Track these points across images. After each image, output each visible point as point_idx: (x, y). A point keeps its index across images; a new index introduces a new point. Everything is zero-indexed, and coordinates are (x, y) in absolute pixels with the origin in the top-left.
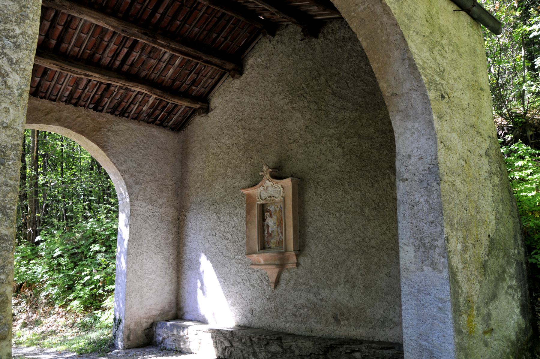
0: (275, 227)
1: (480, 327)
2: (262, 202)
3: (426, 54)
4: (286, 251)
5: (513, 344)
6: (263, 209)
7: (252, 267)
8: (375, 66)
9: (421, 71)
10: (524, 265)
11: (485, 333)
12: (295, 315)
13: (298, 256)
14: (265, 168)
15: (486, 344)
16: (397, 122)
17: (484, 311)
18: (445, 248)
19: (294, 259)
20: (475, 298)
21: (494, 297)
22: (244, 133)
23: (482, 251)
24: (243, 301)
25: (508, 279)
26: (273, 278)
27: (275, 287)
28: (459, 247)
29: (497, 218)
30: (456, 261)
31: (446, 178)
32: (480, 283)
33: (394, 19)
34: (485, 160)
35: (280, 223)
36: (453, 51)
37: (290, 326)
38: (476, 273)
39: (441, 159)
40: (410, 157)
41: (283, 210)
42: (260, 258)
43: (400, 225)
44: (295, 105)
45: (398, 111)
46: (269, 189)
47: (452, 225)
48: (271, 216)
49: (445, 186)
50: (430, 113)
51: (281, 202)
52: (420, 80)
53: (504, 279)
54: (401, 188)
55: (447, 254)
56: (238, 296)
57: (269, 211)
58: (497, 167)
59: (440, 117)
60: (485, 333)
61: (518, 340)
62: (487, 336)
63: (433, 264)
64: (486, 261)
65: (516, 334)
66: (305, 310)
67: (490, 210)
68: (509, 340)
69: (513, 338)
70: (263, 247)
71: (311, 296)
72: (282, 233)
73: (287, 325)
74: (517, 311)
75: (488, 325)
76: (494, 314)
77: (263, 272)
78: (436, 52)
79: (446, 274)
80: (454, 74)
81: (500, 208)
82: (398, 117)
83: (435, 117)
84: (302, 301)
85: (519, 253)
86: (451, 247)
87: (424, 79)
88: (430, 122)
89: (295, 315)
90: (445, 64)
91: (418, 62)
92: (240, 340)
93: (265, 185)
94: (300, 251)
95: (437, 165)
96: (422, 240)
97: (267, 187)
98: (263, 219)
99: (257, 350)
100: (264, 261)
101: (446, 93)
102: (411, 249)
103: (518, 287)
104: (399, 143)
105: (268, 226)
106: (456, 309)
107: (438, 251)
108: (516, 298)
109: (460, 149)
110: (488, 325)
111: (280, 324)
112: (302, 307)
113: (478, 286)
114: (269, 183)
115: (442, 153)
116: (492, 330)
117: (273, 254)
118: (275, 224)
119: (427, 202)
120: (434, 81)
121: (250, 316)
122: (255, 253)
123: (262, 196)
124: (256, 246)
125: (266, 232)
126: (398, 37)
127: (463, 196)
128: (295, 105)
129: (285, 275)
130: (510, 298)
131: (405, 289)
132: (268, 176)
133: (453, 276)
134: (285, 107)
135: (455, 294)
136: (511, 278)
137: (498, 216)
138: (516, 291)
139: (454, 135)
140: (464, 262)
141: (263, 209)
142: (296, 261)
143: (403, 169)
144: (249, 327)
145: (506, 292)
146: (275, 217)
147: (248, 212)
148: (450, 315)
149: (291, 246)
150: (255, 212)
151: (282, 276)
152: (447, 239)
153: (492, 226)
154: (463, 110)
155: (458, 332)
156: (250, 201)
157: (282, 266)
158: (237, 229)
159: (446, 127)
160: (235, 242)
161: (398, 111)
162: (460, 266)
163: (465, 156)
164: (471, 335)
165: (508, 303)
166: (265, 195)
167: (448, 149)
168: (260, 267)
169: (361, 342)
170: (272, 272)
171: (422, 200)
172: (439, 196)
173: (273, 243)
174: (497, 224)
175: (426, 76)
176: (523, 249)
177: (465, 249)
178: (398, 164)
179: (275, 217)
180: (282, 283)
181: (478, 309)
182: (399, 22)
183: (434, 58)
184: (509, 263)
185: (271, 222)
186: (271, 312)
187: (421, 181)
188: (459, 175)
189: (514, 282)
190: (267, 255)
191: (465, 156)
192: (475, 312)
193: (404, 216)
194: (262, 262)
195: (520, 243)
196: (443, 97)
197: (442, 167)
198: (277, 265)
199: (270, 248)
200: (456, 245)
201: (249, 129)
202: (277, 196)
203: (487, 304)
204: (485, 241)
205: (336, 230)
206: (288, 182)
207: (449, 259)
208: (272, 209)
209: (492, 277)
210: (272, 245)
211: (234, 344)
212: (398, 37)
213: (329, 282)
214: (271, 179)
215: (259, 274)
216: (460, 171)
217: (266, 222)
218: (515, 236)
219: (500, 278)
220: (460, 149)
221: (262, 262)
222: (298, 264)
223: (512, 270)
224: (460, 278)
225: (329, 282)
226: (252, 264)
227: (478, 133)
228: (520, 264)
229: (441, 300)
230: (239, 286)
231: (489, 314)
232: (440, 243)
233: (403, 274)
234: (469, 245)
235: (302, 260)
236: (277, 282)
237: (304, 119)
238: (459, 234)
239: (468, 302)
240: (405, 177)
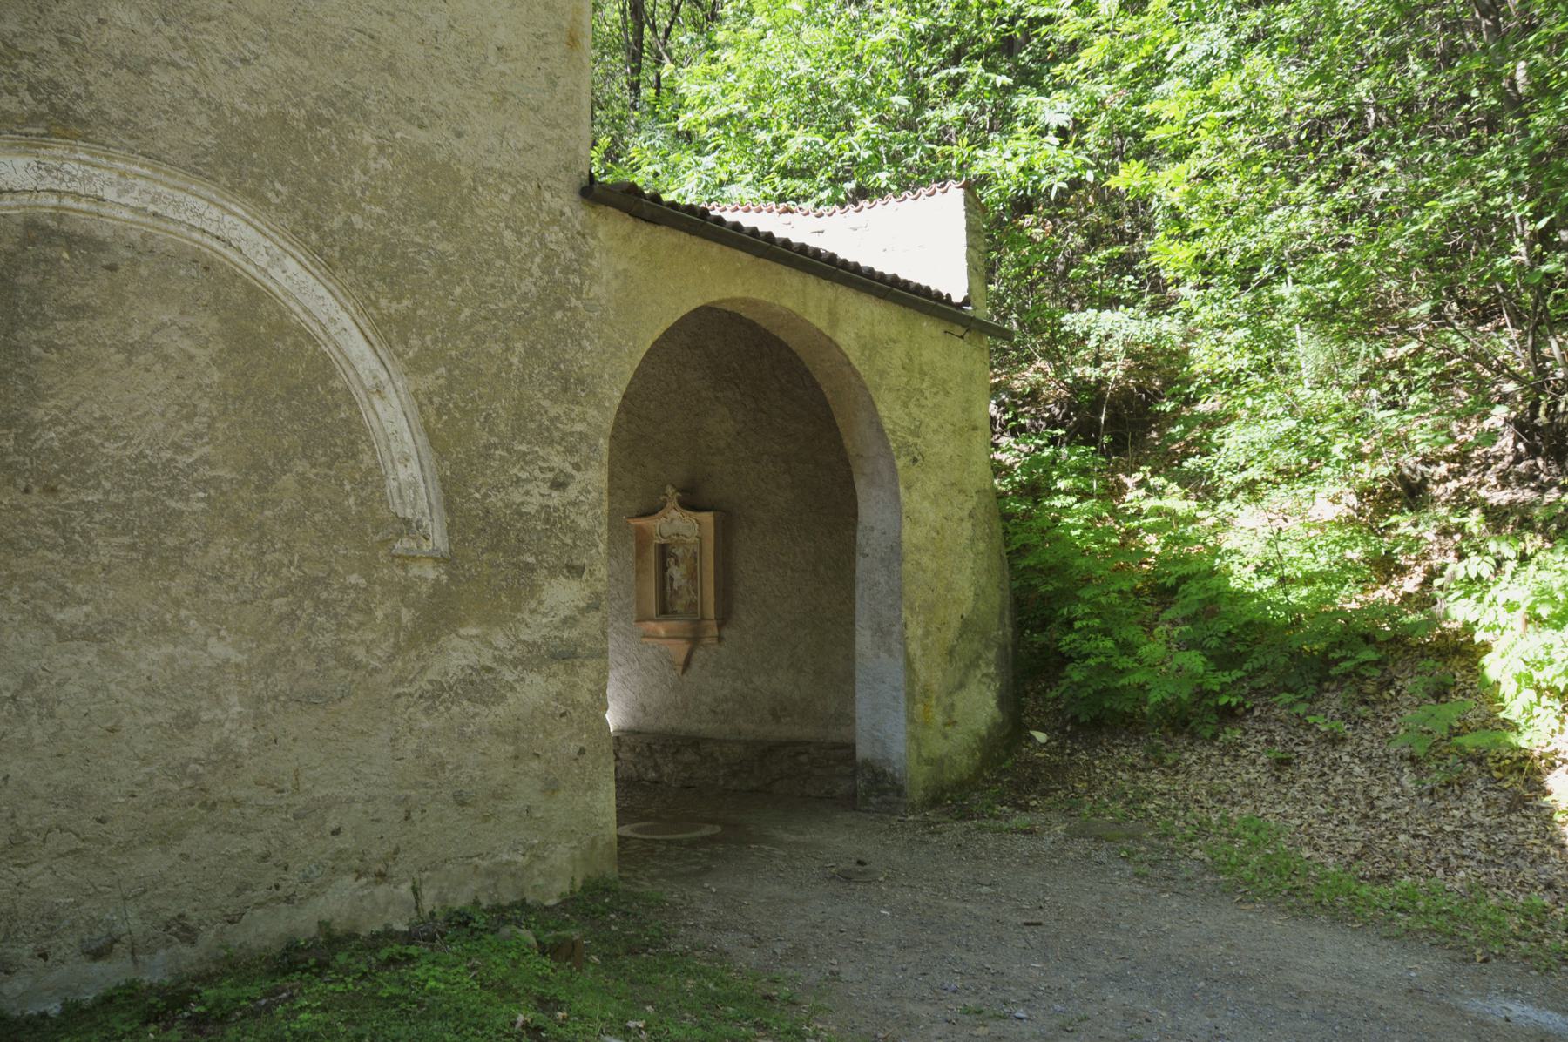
0: (683, 581)
1: (939, 718)
2: (663, 541)
3: (899, 412)
4: (703, 619)
5: (982, 739)
6: (664, 552)
7: (644, 640)
8: (839, 421)
9: (890, 437)
10: (1010, 649)
11: (945, 725)
12: (714, 712)
13: (720, 627)
14: (670, 490)
15: (945, 737)
16: (861, 485)
17: (946, 701)
18: (902, 634)
19: (714, 631)
20: (936, 687)
21: (961, 685)
22: (629, 422)
23: (950, 635)
24: (628, 692)
25: (983, 666)
26: (681, 659)
27: (683, 672)
28: (920, 632)
29: (976, 595)
30: (914, 648)
31: (909, 558)
32: (944, 671)
33: (863, 382)
34: (967, 525)
35: (693, 575)
36: (936, 394)
37: (707, 728)
38: (939, 660)
39: (905, 537)
40: (872, 529)
41: (696, 557)
42: (661, 628)
43: (858, 606)
44: (719, 394)
45: (864, 474)
46: (676, 522)
47: (912, 609)
48: (677, 563)
49: (907, 567)
50: (897, 485)
51: (695, 543)
52: (887, 447)
53: (978, 666)
54: (861, 564)
55: (904, 641)
56: (619, 685)
57: (674, 556)
58: (1302, 237)
59: (908, 488)
60: (945, 725)
61: (990, 735)
62: (947, 728)
63: (889, 651)
64: (955, 646)
65: (989, 728)
66: (731, 704)
67: (967, 585)
68: (978, 735)
69: (984, 731)
70: (665, 610)
71: (739, 684)
72: (696, 593)
73: (702, 727)
74: (993, 703)
75: (949, 717)
76: (960, 705)
77: (663, 648)
78: (911, 405)
79: (901, 661)
80: (934, 425)
81: (983, 581)
82: (862, 481)
83: (902, 488)
84: (726, 692)
85: (1004, 634)
86: (909, 633)
87: (893, 445)
88: (896, 495)
89: (714, 712)
90: (922, 416)
91: (888, 425)
92: (633, 749)
93: (670, 516)
94: (724, 618)
95: (900, 544)
96: (879, 624)
97: (672, 520)
98: (663, 567)
99: (660, 761)
100: (667, 632)
101: (920, 454)
102: (868, 633)
103: (997, 675)
104: (863, 511)
105: (672, 579)
106: (911, 697)
107: (894, 636)
108: (992, 687)
109: (932, 516)
110: (949, 717)
111: (691, 725)
112: (726, 700)
113: (940, 674)
114: (675, 514)
115: (907, 528)
116: (955, 722)
117: (683, 623)
118: (683, 576)
119: (887, 583)
120: (907, 445)
121: (640, 715)
122: (652, 620)
123: (663, 532)
124: (653, 610)
125: (668, 588)
126: (866, 399)
127: (929, 574)
128: (719, 394)
129: (700, 653)
130: (984, 688)
131: (859, 676)
132: (675, 503)
133: (909, 663)
134: (704, 394)
135: (911, 683)
136: (988, 665)
137: (979, 591)
138: (993, 680)
139: (926, 504)
140: (925, 648)
141: (664, 552)
142: (717, 634)
143: (863, 542)
144: (639, 733)
145: (979, 681)
146: (683, 566)
147: (640, 555)
148: (903, 704)
149: (711, 612)
150: (652, 555)
151: (695, 656)
152: (905, 625)
153: (969, 604)
154: (941, 467)
155: (911, 721)
156: (642, 538)
157: (695, 640)
158: (617, 580)
159: (915, 496)
160: (613, 599)
161: (864, 474)
162: (919, 653)
163: (938, 526)
164: (926, 725)
165: (980, 693)
166: (667, 530)
167: (915, 522)
168: (659, 641)
169: (809, 743)
170: (679, 649)
171: (882, 580)
172: (900, 578)
173: (679, 605)
174: (976, 601)
175: (895, 441)
176: (1011, 629)
177: (927, 634)
178: (859, 535)
179: (683, 566)
180: (695, 665)
181: (938, 698)
182: (868, 384)
183: (909, 415)
184: (987, 647)
185: (677, 573)
186: (676, 708)
187: (883, 559)
188: (927, 550)
189: (992, 670)
190: (673, 624)
191: (938, 526)
192: (934, 702)
193: (862, 595)
194: (662, 633)
195: (1007, 621)
196: (915, 460)
197: (905, 546)
198: (688, 639)
199: (675, 612)
200: (915, 630)
201: (639, 417)
202: (688, 534)
203: (950, 694)
204: (956, 624)
205: (777, 593)
206: (707, 518)
207: (905, 646)
208: (679, 552)
209: (961, 664)
210: (679, 608)
211: (621, 755)
212: (866, 399)
213: (765, 665)
214: (678, 508)
215: (656, 651)
216: (929, 545)
217: (668, 573)
218: (1001, 615)
219: (973, 664)
220: (932, 516)
221: (662, 633)
222: (720, 639)
223: (992, 655)
224: (917, 665)
225: (765, 665)
226: (644, 636)
227: (960, 491)
228: (1002, 648)
229: (895, 689)
230: (621, 669)
231: (952, 705)
232: (897, 628)
233: (858, 660)
234: (933, 628)
235: (726, 632)
236: (687, 664)
237: (735, 420)
238: (921, 618)
239: (926, 692)
240: (866, 551)
